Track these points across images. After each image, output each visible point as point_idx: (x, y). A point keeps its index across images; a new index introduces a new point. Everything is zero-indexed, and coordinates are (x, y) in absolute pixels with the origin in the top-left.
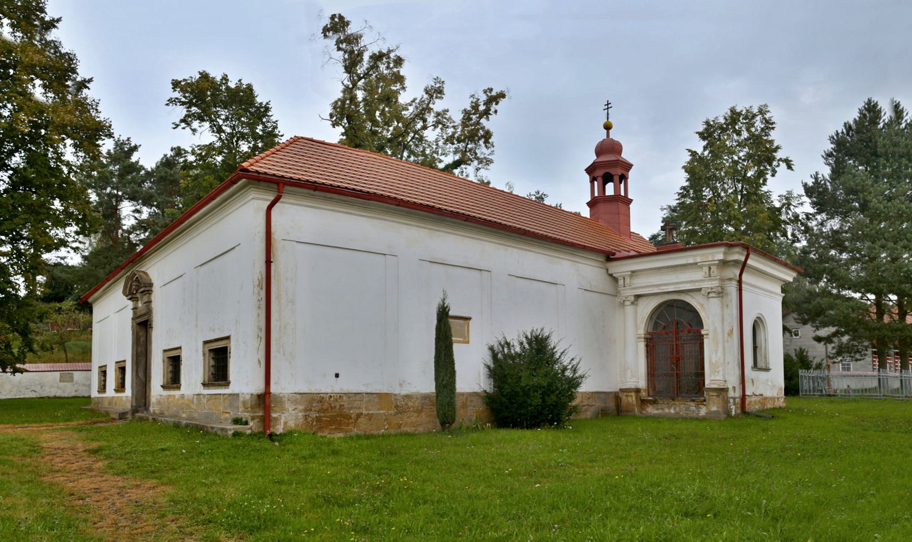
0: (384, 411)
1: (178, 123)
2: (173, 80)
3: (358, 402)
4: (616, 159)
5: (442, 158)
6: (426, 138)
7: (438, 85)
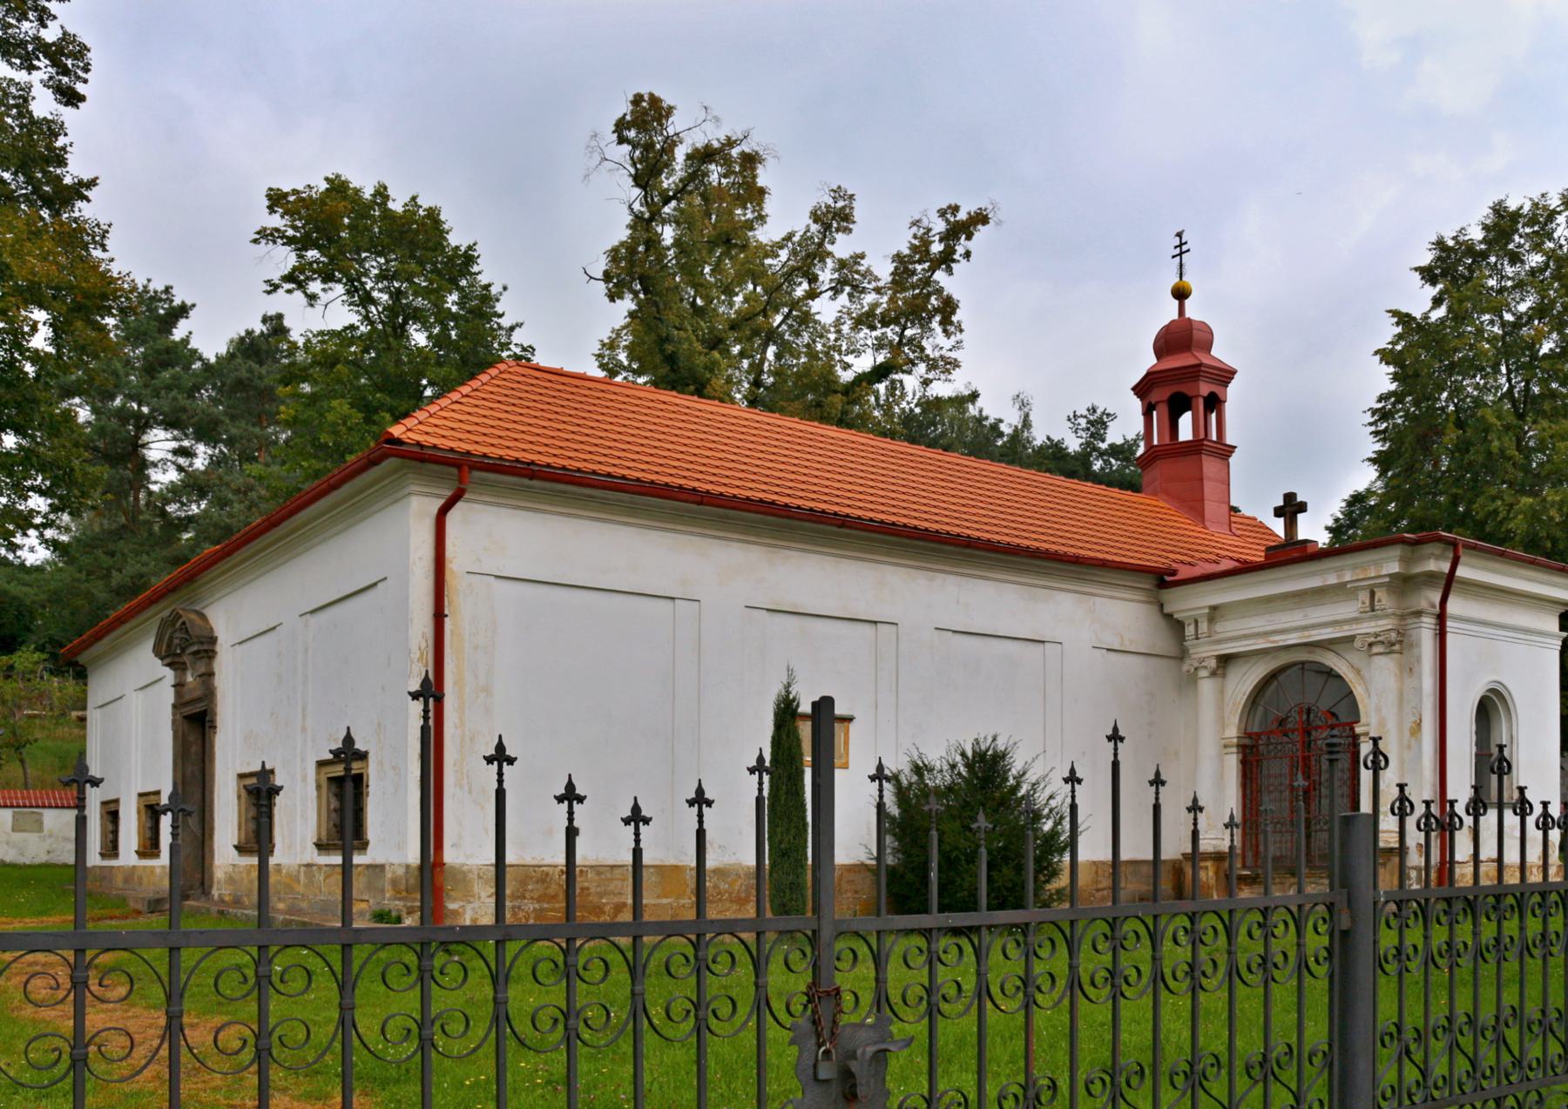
0: (668, 901)
1: (277, 282)
2: (271, 189)
3: (619, 883)
4: (1194, 362)
5: (849, 359)
6: (817, 317)
7: (840, 204)
